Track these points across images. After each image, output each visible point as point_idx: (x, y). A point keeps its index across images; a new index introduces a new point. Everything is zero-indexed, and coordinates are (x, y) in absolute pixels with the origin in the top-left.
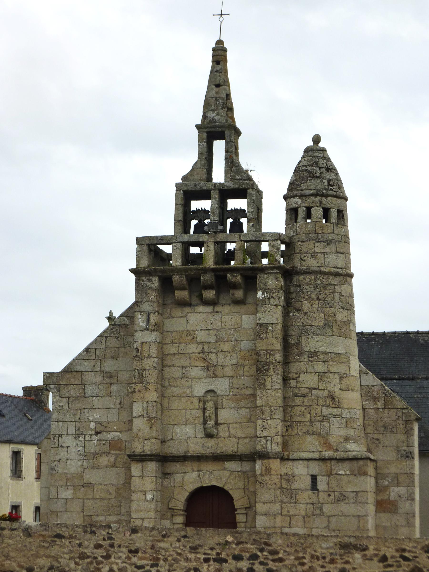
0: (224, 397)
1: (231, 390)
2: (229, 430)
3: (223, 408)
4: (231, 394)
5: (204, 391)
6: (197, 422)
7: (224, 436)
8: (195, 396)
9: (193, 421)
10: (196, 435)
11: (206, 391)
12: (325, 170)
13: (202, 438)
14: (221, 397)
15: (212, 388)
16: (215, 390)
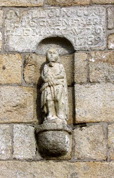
3: (89, 81)
5: (38, 38)
6: (15, 117)
8: (14, 52)
11: (42, 38)
16: (71, 38)
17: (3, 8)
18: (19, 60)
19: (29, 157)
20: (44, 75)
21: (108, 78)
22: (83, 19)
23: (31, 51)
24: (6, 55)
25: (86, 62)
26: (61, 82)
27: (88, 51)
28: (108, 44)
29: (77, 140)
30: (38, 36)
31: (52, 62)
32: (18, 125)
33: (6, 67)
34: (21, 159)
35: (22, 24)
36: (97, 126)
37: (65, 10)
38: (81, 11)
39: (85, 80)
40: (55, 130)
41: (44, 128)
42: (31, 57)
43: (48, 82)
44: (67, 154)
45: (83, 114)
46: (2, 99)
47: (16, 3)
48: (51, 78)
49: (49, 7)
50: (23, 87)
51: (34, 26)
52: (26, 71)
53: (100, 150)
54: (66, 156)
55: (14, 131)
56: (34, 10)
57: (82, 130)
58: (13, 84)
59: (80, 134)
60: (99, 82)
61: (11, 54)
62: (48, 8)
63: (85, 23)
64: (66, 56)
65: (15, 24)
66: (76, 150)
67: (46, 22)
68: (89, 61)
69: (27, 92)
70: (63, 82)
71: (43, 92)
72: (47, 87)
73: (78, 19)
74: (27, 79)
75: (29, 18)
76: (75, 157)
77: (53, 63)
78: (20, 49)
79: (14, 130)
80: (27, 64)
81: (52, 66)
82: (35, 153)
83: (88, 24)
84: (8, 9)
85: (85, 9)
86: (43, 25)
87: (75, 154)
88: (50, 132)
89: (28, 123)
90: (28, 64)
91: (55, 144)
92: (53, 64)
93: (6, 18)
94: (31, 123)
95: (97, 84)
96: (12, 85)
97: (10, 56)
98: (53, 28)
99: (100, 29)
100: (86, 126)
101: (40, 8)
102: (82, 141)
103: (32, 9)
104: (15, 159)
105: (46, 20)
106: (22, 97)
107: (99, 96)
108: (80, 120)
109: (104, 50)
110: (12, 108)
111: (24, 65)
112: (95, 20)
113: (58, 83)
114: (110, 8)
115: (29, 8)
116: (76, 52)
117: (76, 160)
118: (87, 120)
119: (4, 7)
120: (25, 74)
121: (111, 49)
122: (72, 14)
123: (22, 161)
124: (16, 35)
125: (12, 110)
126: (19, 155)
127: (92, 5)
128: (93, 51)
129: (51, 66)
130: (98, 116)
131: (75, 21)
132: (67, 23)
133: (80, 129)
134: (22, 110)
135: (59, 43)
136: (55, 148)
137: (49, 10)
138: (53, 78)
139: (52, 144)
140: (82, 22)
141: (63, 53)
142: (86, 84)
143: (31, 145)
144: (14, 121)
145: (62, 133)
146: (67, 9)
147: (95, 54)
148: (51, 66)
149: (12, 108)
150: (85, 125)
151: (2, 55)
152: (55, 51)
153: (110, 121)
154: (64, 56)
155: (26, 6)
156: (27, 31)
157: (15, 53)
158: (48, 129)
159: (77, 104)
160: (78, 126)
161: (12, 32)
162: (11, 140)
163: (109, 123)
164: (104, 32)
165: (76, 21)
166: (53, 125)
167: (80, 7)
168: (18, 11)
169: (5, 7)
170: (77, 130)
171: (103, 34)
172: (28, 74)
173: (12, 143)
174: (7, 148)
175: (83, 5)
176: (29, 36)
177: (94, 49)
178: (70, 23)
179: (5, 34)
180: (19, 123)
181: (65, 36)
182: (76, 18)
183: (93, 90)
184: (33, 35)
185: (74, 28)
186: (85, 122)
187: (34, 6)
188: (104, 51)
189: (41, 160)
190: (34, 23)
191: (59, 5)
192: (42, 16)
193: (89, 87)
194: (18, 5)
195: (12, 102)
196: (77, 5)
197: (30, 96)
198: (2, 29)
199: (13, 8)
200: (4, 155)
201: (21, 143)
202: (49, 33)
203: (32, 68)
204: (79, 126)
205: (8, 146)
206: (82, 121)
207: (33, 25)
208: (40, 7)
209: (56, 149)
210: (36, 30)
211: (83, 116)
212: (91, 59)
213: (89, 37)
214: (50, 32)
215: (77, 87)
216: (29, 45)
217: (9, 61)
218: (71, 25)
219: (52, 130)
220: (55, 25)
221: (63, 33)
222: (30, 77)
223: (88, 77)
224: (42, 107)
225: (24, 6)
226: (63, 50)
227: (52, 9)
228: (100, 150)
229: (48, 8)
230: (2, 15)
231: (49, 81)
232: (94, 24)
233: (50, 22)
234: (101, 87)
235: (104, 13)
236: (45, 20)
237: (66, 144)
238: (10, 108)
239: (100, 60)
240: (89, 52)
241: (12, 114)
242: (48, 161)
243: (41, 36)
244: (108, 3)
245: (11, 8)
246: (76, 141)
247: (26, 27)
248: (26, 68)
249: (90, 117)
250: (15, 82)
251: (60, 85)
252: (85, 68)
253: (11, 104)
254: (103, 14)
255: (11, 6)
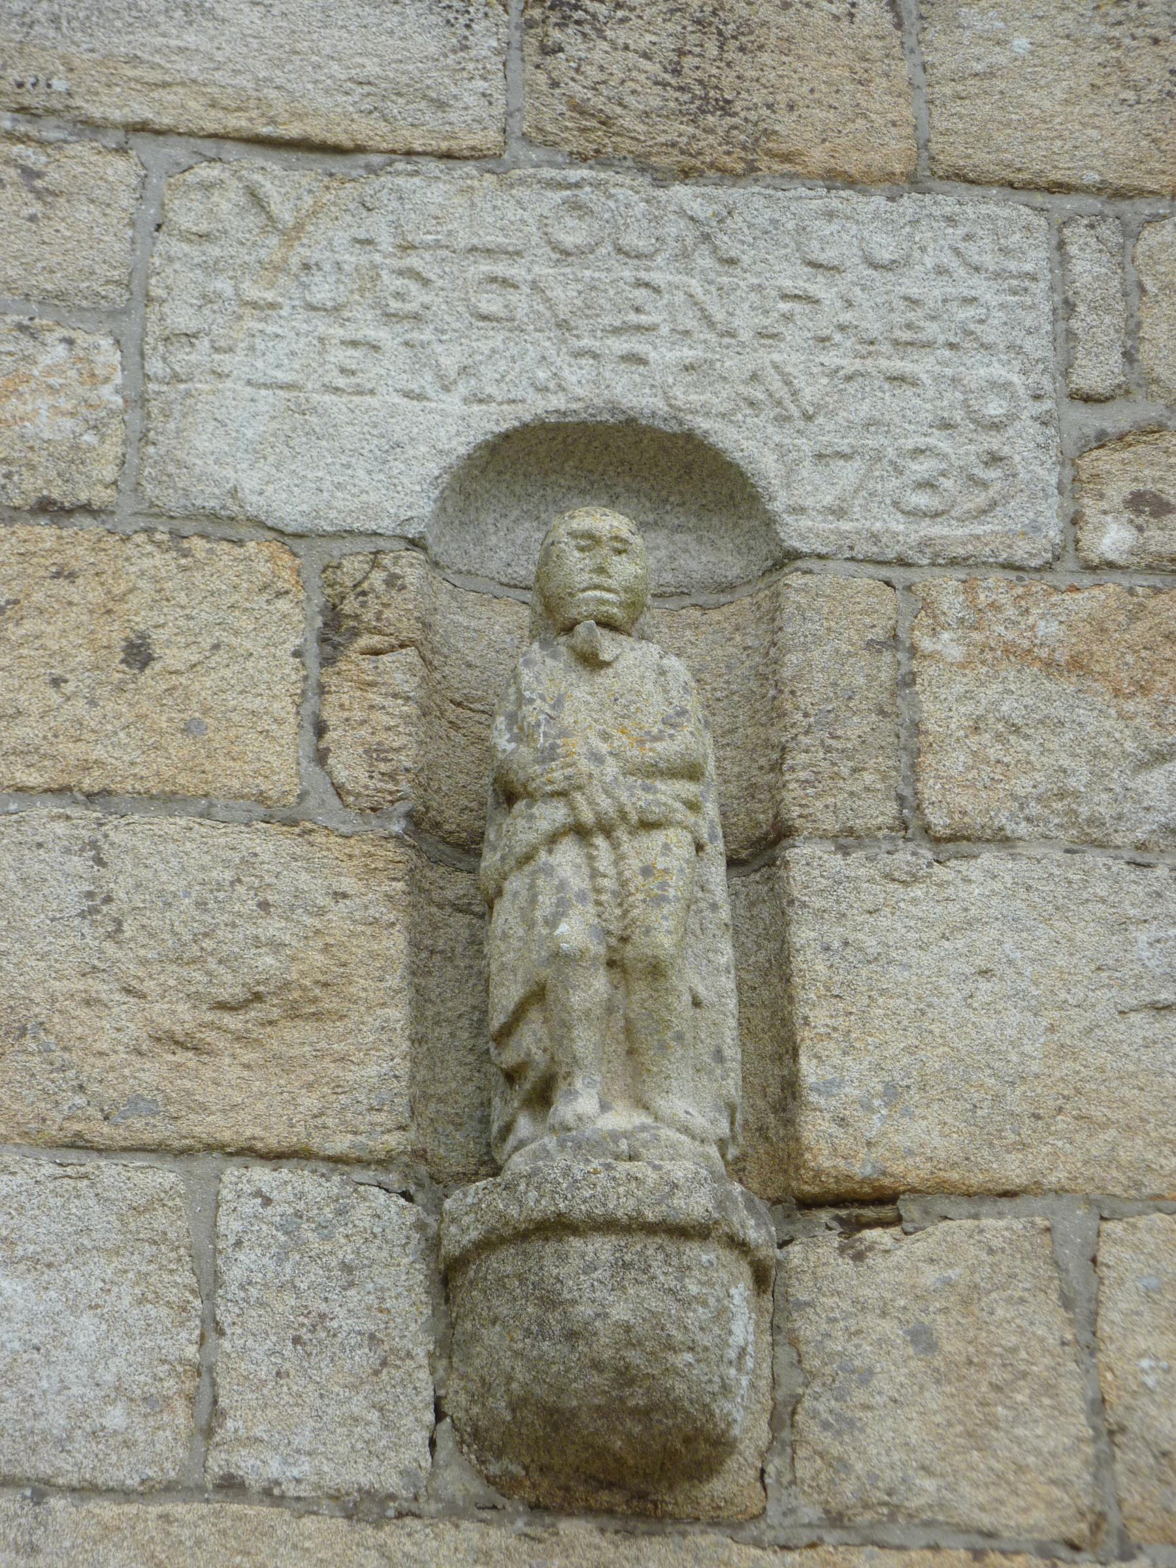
0: (949, 595)
1: (1120, 471)
2: (1089, 1344)
3: (911, 825)
4: (1113, 538)
5: (455, 427)
6: (236, 1094)
7: (972, 1503)
8: (226, 524)
9: (151, 1073)
10: (208, 1427)
11: (491, 421)
12: (422, 1354)
13: (363, 1507)
14: (869, 603)
15: (645, 386)
16: (747, 442)
17: (138, 141)
18: (279, 595)
19: (365, 1480)
20: (523, 735)
21: (1084, 811)
22: (857, 290)
23: (387, 522)
24: (158, 544)
25: (887, 657)
26: (678, 805)
27: (903, 562)
28: (1076, 520)
29: (820, 1345)
30: (453, 403)
31: (599, 623)
32: (262, 1175)
33: (157, 651)
34: (292, 1490)
35: (306, 286)
36: (1001, 1223)
37: (696, 208)
38: (834, 227)
39: (883, 812)
40: (651, 1229)
41: (536, 1204)
42: (392, 581)
43: (562, 794)
44: (731, 1464)
45: (868, 1108)
46: (119, 930)
47: (252, 103)
48: (597, 758)
49: (552, 164)
50: (319, 838)
51: (416, 317)
52: (343, 693)
53: (1037, 1452)
54: (717, 1487)
55: (229, 1225)
56: (416, 180)
57: (859, 1257)
58: (221, 803)
59: (841, 1287)
60: (1003, 840)
61: (203, 536)
62: (547, 173)
63: (873, 326)
64: (687, 601)
65: (245, 285)
66: (814, 1432)
67: (526, 289)
68: (913, 651)
69: (347, 884)
70: (693, 806)
71: (515, 884)
72: (552, 839)
73: (812, 289)
74: (347, 766)
75: (369, 242)
76: (802, 1500)
77: (605, 632)
78: (291, 510)
79: (222, 1221)
80: (355, 633)
81: (606, 656)
82: (420, 1438)
83: (898, 334)
84: (177, 151)
85: (876, 216)
86: (503, 313)
87: (804, 1470)
88: (601, 1247)
89: (359, 1161)
90: (364, 641)
91: (634, 1357)
92: (608, 646)
93: (159, 227)
94: (384, 1162)
95: (988, 858)
96: (211, 805)
97: (201, 555)
98: (586, 342)
99: (1001, 387)
100: (898, 1220)
101: (470, 168)
102: (865, 1353)
103: (398, 173)
104: (231, 1486)
105: (529, 278)
106: (308, 920)
107: (1010, 962)
108: (841, 1163)
109: (1048, 567)
110: (209, 1016)
111: (323, 640)
112: (966, 314)
113: (655, 813)
114: (1092, 226)
115: (376, 159)
116: (799, 563)
117: (810, 1525)
118: (913, 1171)
119: (141, 128)
120: (331, 716)
121: (1111, 565)
122: (761, 244)
123: (304, 1507)
124: (257, 377)
125: (210, 1036)
126: (267, 1455)
127: (936, 184)
128: (949, 572)
129: (591, 661)
130: (1012, 1137)
131: (784, 306)
132: (719, 316)
133: (842, 1250)
134: (297, 1037)
135: (628, 489)
136: (637, 1399)
137: (558, 196)
138: (610, 760)
139: (607, 1354)
140: (846, 317)
141: (668, 577)
142: (886, 846)
143: (384, 1363)
144: (227, 1136)
145: (704, 1258)
146: (711, 199)
147: (965, 592)
148: (591, 661)
149: (209, 1016)
150: (887, 1212)
151: (126, 539)
152: (606, 541)
153: (1118, 1190)
154: (671, 604)
155: (351, 144)
156: (351, 352)
157: (243, 530)
158: (580, 1210)
159: (816, 1015)
160: (825, 1216)
161: (217, 350)
162: (197, 1303)
163: (1105, 1209)
164: (1044, 421)
165: (797, 307)
166: (631, 1178)
167: (829, 189)
168: (276, 179)
169: (158, 133)
170: (817, 1254)
171: (1034, 429)
172: (363, 722)
173: (202, 1336)
174: (155, 1377)
175: (851, 183)
176: (372, 392)
177: (961, 552)
178: (745, 322)
179: (155, 366)
180: (275, 1157)
181: (703, 424)
182: (794, 277)
183: (953, 908)
184: (408, 395)
185: (776, 357)
186: (886, 1181)
187: (417, 146)
188: (1048, 577)
189: (487, 1509)
190: (414, 287)
191: (642, 165)
192: (492, 239)
193: (916, 879)
194: (272, 121)
195: (212, 963)
196: (793, 176)
197: (376, 921)
198: (125, 312)
199: (229, 145)
200: (126, 1444)
201: (296, 1340)
202: (552, 385)
203: (399, 670)
204: (838, 1219)
205: (163, 1362)
206: (868, 1170)
207: (410, 307)
208: (472, 163)
209: (643, 1414)
210: (439, 349)
211: (874, 1125)
212: (934, 633)
213: (910, 444)
214: (575, 385)
215: (807, 861)
216: (369, 472)
217: (182, 598)
218: (745, 336)
219: (608, 1225)
220: (606, 320)
221: (678, 392)
222: (375, 753)
223: (907, 792)
224: (497, 1021)
225: (331, 139)
226: (662, 553)
227: (577, 185)
228: (1037, 1452)
229: (547, 173)
230: (126, 200)
231: (579, 788)
232: (952, 346)
233: (557, 293)
234: (1028, 888)
235: (1036, 258)
236: (515, 271)
237: (733, 1372)
238: (185, 1017)
239: (1009, 650)
240: (912, 575)
241: (208, 1073)
242: (548, 1520)
243: (476, 408)
244: (1073, 181)
245: (209, 147)
246: (810, 1349)
247: (346, 314)
248: (342, 666)
249: (937, 1141)
250: (236, 784)
251: (671, 832)
252: (881, 712)
253: (198, 976)
254: (1028, 267)
255: (211, 127)
